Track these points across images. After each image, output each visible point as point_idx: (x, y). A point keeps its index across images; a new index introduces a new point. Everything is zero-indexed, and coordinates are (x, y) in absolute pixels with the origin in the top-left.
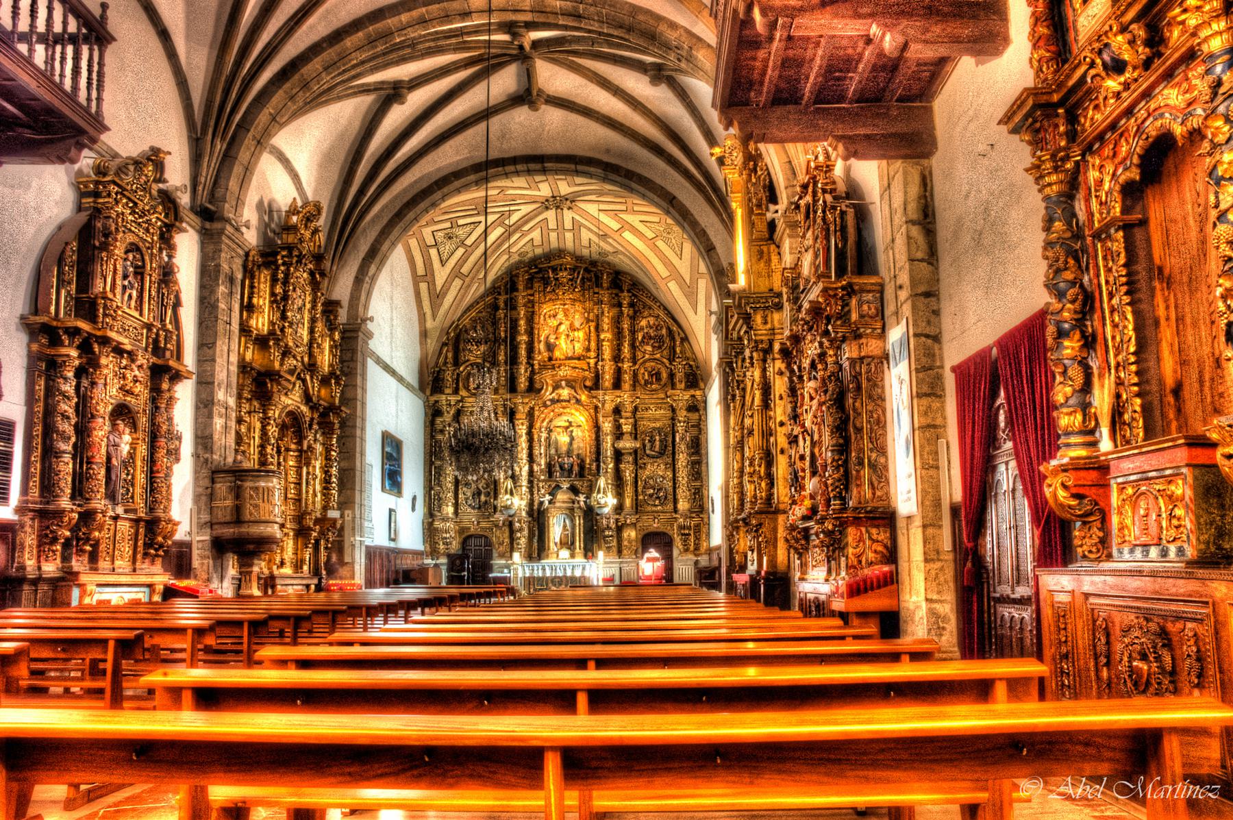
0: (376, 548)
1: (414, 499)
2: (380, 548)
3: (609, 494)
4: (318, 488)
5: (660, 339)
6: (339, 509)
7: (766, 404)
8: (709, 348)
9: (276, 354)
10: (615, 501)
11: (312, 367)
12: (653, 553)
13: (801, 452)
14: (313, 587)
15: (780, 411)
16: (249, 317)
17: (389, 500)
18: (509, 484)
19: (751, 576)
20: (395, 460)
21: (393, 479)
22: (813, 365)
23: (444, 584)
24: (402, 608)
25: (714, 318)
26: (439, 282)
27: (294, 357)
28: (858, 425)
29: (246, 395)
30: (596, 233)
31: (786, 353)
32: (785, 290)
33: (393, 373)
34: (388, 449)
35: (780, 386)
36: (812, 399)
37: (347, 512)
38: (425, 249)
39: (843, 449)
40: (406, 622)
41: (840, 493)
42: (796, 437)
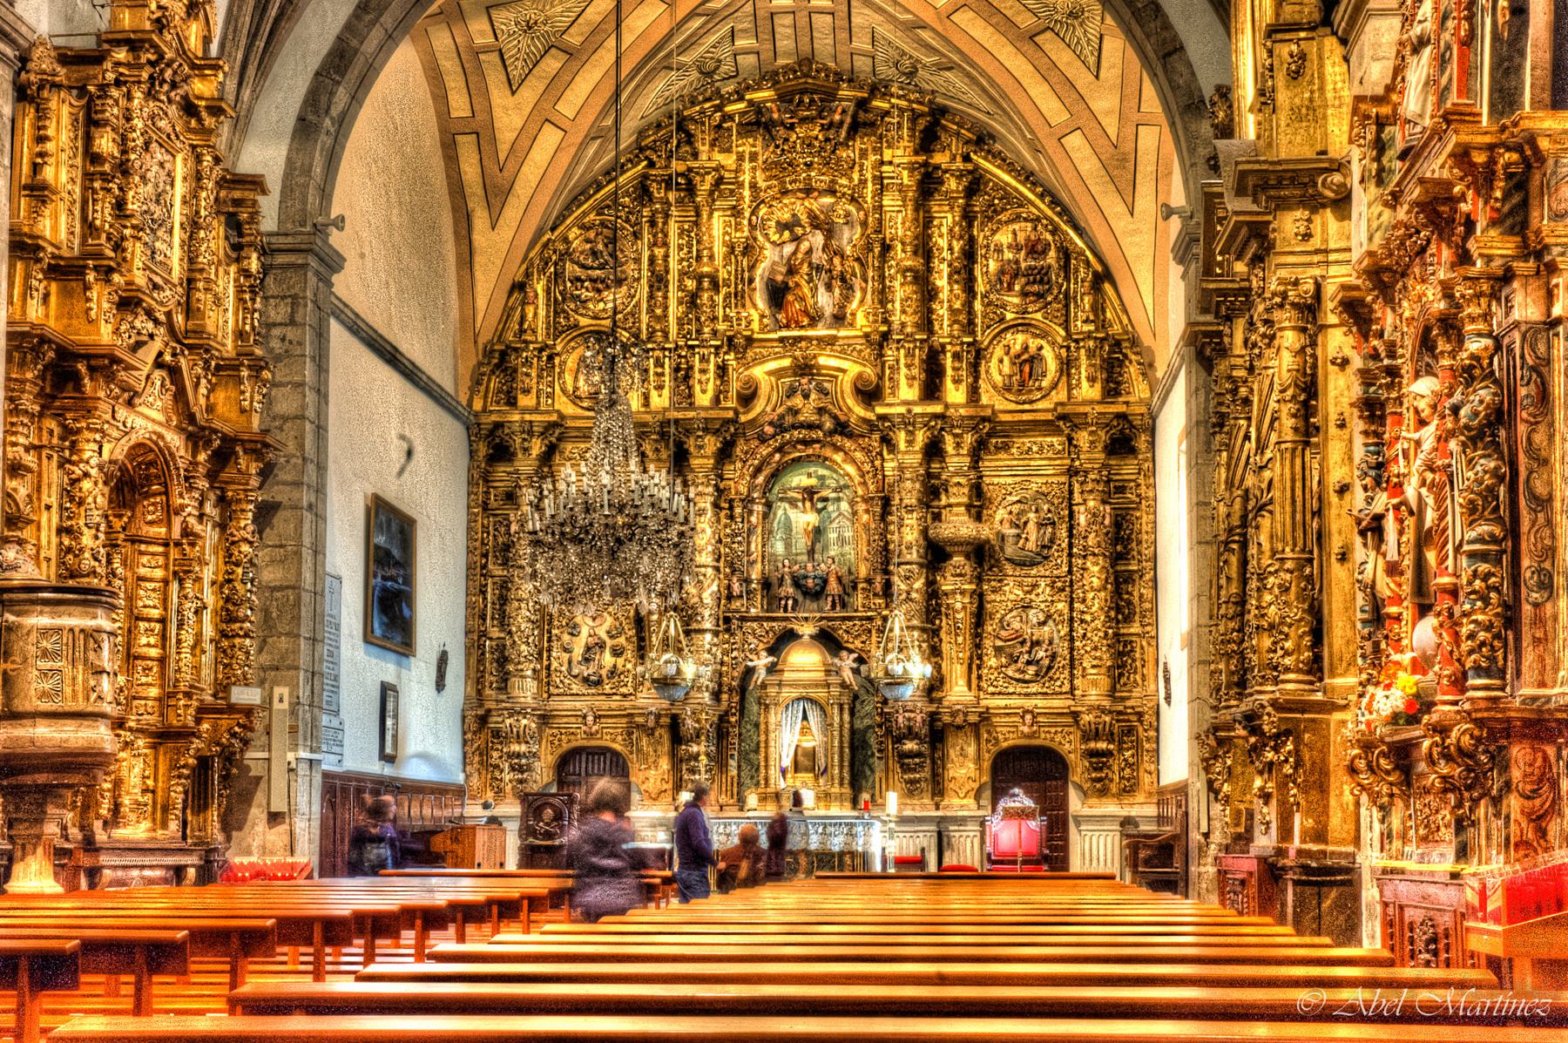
0: (347, 777)
1: (443, 660)
2: (360, 778)
3: (915, 654)
4: (209, 631)
5: (1041, 276)
6: (261, 683)
7: (1309, 431)
8: (1160, 303)
9: (100, 299)
10: (928, 670)
11: (192, 340)
12: (1021, 799)
13: (1392, 555)
14: (192, 872)
15: (1342, 456)
16: (35, 213)
17: (386, 668)
18: (673, 626)
19: (1262, 860)
20: (397, 564)
21: (391, 614)
22: (1556, 142)
23: (511, 865)
24: (361, 933)
25: (1175, 224)
26: (506, 136)
27: (149, 313)
28: (1540, 489)
29: (29, 403)
30: (892, 19)
31: (1357, 313)
32: (1356, 153)
33: (390, 356)
34: (380, 540)
35: (1340, 391)
36: (1422, 423)
37: (277, 691)
38: (470, 59)
39: (1505, 548)
40: (420, 956)
41: (1492, 659)
42: (1379, 518)
